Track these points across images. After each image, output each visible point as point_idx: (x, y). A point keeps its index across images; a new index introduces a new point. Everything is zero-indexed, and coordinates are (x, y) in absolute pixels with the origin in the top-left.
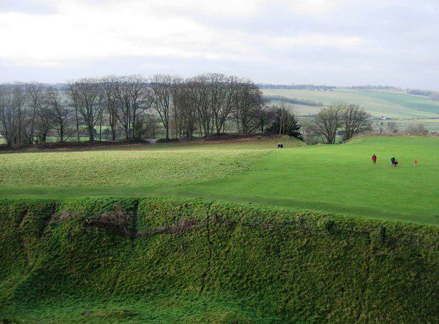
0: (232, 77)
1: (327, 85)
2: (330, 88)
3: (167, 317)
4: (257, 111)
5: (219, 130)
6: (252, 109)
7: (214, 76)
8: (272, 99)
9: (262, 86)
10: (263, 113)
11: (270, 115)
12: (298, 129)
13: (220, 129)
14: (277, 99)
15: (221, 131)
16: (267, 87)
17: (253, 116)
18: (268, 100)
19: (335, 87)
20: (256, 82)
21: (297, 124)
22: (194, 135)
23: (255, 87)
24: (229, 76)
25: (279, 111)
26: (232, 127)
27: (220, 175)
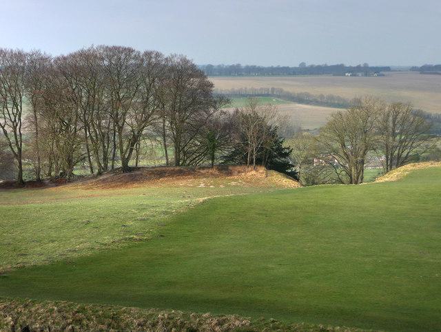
0: (148, 54)
1: (370, 65)
2: (378, 71)
3: (316, 328)
4: (203, 123)
5: (125, 161)
6: (192, 118)
7: (114, 51)
8: (233, 98)
9: (211, 70)
10: (217, 124)
11: (230, 126)
12: (286, 155)
13: (128, 159)
14: (240, 95)
15: (131, 163)
16: (234, 71)
17: (196, 130)
18: (224, 99)
19: (387, 69)
20: (199, 61)
21: (284, 145)
22: (76, 172)
23: (194, 72)
24: (142, 52)
25: (246, 119)
26: (154, 152)
27: (74, 261)
